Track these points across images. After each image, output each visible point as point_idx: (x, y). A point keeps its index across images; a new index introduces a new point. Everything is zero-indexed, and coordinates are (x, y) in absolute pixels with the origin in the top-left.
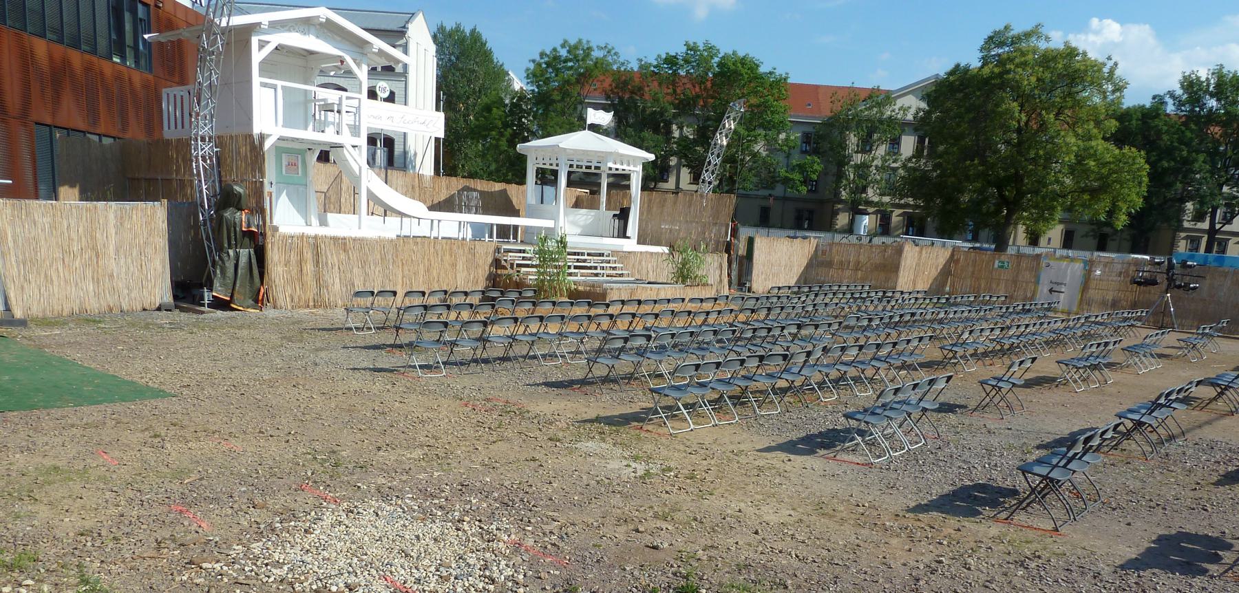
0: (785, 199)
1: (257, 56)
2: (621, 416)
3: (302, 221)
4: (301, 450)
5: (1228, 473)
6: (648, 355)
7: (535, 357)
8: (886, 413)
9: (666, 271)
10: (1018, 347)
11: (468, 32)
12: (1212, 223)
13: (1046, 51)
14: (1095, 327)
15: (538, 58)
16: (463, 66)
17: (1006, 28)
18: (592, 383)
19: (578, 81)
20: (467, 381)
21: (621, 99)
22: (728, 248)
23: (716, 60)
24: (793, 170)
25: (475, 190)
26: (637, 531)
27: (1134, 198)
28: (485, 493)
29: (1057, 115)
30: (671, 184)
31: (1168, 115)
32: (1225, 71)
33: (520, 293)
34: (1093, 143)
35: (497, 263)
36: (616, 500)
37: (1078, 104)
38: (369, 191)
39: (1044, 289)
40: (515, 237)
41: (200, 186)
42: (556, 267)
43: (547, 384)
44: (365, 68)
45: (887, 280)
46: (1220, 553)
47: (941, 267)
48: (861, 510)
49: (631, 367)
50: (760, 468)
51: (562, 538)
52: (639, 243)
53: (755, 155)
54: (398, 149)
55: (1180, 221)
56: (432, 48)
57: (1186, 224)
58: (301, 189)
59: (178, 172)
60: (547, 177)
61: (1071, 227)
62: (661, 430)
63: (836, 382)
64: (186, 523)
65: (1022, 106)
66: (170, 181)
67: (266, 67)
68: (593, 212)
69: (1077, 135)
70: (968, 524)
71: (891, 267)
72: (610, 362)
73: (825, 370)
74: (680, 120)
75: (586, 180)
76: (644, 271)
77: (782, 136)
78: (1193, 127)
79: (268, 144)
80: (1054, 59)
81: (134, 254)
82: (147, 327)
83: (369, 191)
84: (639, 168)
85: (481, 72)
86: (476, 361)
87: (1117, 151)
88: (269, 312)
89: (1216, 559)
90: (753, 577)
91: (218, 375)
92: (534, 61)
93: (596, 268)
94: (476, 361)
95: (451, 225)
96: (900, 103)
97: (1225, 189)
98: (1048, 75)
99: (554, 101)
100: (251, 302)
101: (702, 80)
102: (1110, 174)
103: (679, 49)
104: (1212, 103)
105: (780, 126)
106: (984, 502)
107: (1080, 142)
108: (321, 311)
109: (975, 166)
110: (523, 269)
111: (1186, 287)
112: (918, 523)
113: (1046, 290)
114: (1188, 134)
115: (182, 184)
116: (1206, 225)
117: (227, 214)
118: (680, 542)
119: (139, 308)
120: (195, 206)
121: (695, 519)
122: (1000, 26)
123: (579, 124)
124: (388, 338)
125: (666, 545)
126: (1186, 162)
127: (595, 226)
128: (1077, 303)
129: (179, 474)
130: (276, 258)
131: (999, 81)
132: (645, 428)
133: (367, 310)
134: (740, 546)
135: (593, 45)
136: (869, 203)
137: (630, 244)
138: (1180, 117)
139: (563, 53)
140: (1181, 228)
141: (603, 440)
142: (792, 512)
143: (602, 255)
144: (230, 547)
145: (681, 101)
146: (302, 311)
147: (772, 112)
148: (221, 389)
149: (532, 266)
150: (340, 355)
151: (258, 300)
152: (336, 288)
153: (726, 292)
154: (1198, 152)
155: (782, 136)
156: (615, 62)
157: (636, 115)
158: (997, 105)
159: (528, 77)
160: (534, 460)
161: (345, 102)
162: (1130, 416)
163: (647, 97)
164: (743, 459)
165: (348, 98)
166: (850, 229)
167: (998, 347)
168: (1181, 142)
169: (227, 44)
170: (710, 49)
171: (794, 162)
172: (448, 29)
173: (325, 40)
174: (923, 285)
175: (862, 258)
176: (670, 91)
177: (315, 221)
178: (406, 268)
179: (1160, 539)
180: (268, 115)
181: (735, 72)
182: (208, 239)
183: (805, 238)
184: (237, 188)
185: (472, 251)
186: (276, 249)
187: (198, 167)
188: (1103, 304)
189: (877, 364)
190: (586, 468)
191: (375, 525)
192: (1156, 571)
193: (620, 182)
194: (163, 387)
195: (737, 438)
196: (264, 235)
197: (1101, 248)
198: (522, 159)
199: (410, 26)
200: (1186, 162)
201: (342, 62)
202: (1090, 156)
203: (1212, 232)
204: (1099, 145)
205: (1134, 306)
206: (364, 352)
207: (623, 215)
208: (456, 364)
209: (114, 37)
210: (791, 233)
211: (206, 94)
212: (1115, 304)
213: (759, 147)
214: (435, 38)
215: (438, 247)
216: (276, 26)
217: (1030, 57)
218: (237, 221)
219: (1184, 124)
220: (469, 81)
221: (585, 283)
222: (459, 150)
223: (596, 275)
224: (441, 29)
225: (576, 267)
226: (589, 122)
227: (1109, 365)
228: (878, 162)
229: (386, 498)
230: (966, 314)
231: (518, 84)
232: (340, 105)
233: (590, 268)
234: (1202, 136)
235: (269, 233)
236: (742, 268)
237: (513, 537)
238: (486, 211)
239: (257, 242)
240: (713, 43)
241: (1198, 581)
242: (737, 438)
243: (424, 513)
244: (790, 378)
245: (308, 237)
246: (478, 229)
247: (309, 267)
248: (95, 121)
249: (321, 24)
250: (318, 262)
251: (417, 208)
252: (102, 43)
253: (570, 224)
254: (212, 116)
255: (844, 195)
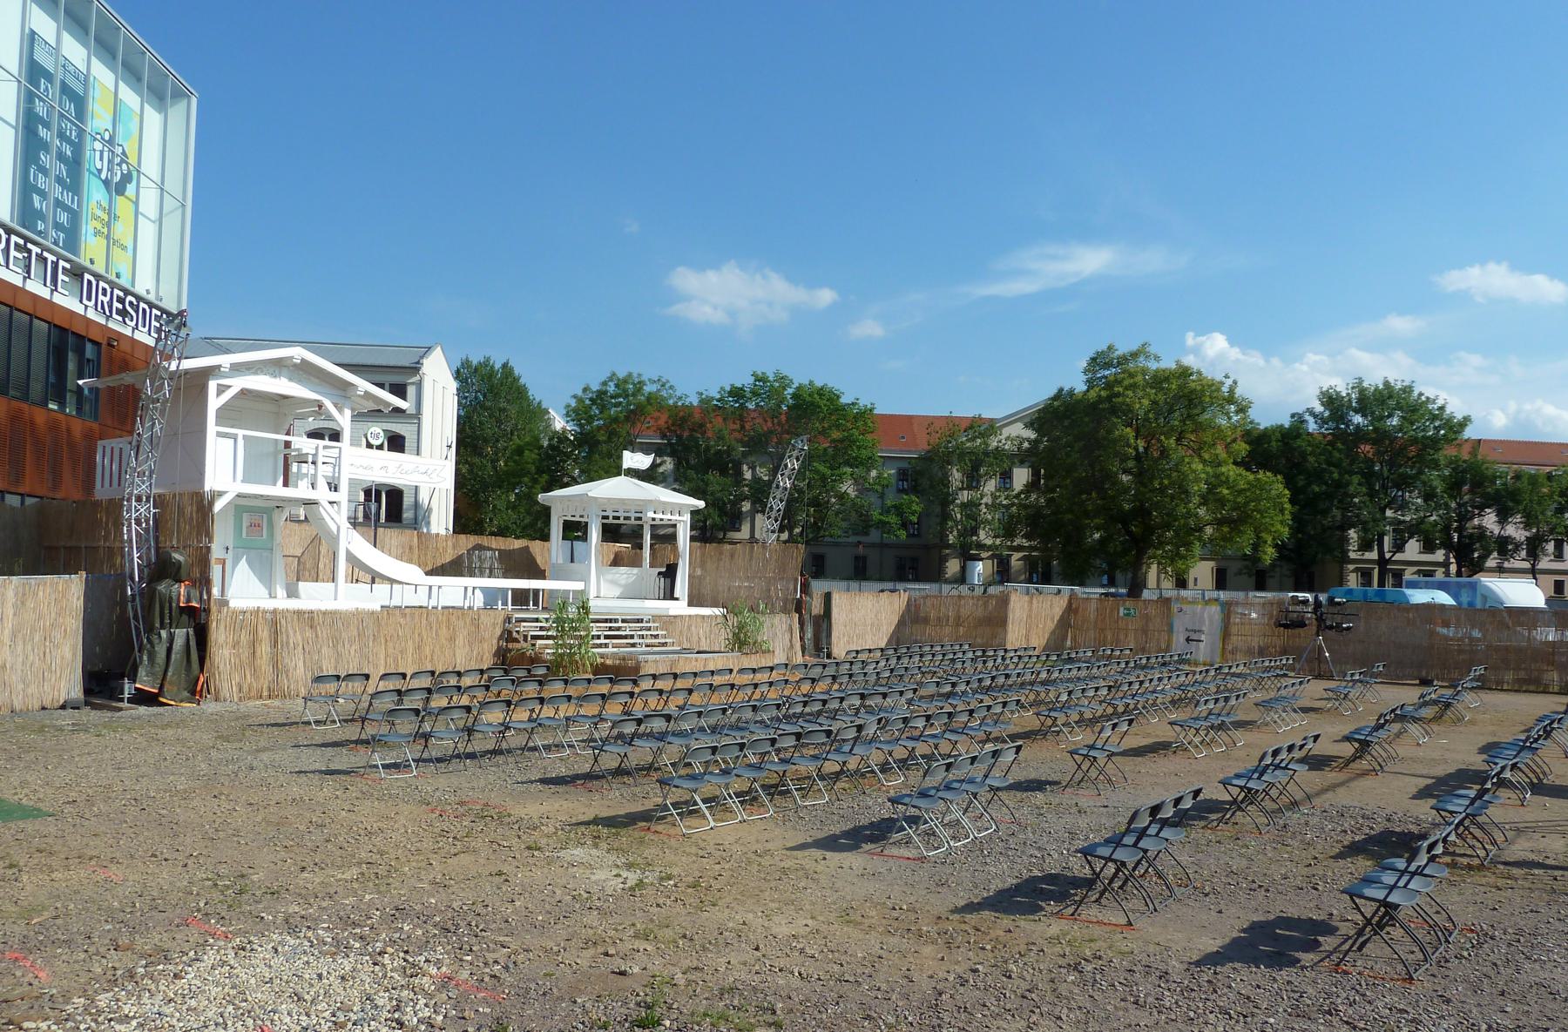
0: (882, 546)
1: (214, 403)
2: (628, 815)
3: (264, 592)
4: (201, 875)
5: (1353, 843)
6: (670, 739)
7: (535, 749)
8: (940, 794)
9: (721, 638)
10: (1136, 708)
11: (498, 366)
12: (1381, 553)
13: (1157, 371)
14: (1231, 682)
15: (580, 393)
16: (490, 402)
17: (1110, 348)
18: (603, 777)
19: (627, 418)
20: (442, 782)
21: (679, 437)
22: (799, 607)
23: (790, 391)
24: (888, 512)
25: (489, 549)
26: (607, 954)
27: (1280, 526)
28: (424, 918)
29: (1178, 440)
30: (744, 533)
31: (1309, 434)
32: (1365, 384)
33: (529, 671)
34: (1224, 469)
35: (508, 636)
36: (592, 918)
37: (1199, 428)
38: (348, 553)
39: (1179, 639)
40: (536, 604)
41: (131, 554)
42: (576, 637)
43: (543, 781)
44: (348, 413)
45: (994, 636)
46: (1320, 939)
47: (1057, 618)
48: (895, 914)
49: (641, 752)
50: (784, 871)
51: (506, 968)
52: (690, 604)
53: (842, 497)
54: (408, 501)
55: (1345, 552)
56: (453, 386)
57: (1352, 555)
58: (265, 554)
59: (106, 538)
60: (575, 530)
61: (1223, 564)
62: (672, 831)
63: (903, 764)
64: (18, 973)
65: (1137, 431)
66: (96, 549)
67: (224, 415)
68: (635, 570)
69: (1204, 462)
70: (1024, 923)
71: (997, 620)
72: (622, 751)
73: (886, 748)
74: (751, 459)
75: (621, 533)
76: (695, 639)
77: (874, 473)
78: (1339, 445)
79: (218, 506)
80: (1167, 379)
81: (37, 639)
82: (41, 730)
83: (348, 553)
84: (687, 517)
85: (513, 410)
86: (458, 756)
87: (1251, 477)
88: (209, 706)
89: (1313, 946)
90: (736, 1002)
91: (118, 788)
92: (575, 397)
93: (632, 637)
94: (458, 756)
95: (454, 591)
96: (1006, 432)
97: (1389, 513)
98: (1161, 398)
99: (598, 442)
100: (186, 694)
101: (775, 413)
102: (1247, 504)
103: (745, 380)
104: (1358, 419)
105: (868, 463)
106: (1048, 896)
107: (1209, 469)
108: (276, 703)
109: (1092, 500)
110: (539, 642)
111: (1338, 628)
112: (963, 926)
113: (1182, 639)
114: (1337, 454)
115: (111, 552)
116: (1374, 555)
117: (161, 587)
118: (656, 966)
119: (37, 706)
120: (123, 578)
121: (684, 936)
122: (1103, 347)
123: (615, 470)
124: (352, 732)
125: (636, 970)
126: (1339, 485)
127: (632, 590)
128: (1219, 651)
129: (28, 913)
130: (221, 639)
131: (1107, 406)
132: (653, 828)
133: (334, 698)
134: (733, 965)
135: (645, 378)
136: (980, 546)
137: (679, 607)
138: (1325, 436)
139: (611, 388)
140: (1346, 560)
141: (596, 846)
142: (810, 922)
143: (641, 621)
144: (67, 1001)
145: (752, 438)
146: (251, 703)
147: (859, 448)
148: (117, 804)
149: (548, 638)
150: (287, 757)
151: (195, 692)
152: (299, 672)
153: (799, 659)
154: (1351, 473)
155: (874, 473)
156: (671, 397)
157: (698, 455)
158: (1109, 432)
159: (567, 415)
160: (500, 874)
161: (321, 452)
162: (1235, 782)
163: (710, 434)
164: (766, 861)
165: (325, 447)
166: (962, 578)
167: (1110, 710)
168: (1330, 464)
169: (176, 391)
170: (783, 381)
171: (889, 503)
172: (475, 363)
173: (299, 382)
174: (1038, 641)
175: (965, 612)
176: (737, 427)
177: (281, 592)
178: (390, 644)
179: (1254, 927)
180: (225, 468)
181: (812, 404)
182: (136, 617)
183: (892, 591)
184: (176, 556)
185: (476, 623)
186: (222, 627)
187: (129, 531)
188: (1250, 652)
189: (953, 737)
190: (564, 881)
191: (270, 963)
192: (1238, 965)
193: (664, 536)
194: (40, 805)
195: (766, 835)
196: (207, 611)
197: (1260, 587)
198: (546, 512)
199: (425, 361)
200: (1339, 485)
201: (320, 407)
202: (1222, 483)
203: (1382, 562)
204: (1230, 470)
205: (1284, 652)
206: (319, 751)
207: (670, 573)
208: (430, 760)
209: (52, 379)
210: (890, 585)
211: (145, 447)
212: (1262, 652)
213: (848, 487)
214: (458, 375)
215: (432, 618)
216: (238, 369)
217: (1139, 378)
218: (174, 595)
219: (1330, 443)
220: (499, 421)
221: (614, 655)
222: (486, 502)
223: (633, 645)
224: (466, 364)
225: (607, 637)
226: (625, 466)
227: (1239, 725)
228: (987, 500)
229: (293, 930)
230: (1075, 672)
231: (559, 423)
232: (315, 455)
233: (625, 637)
234: (1354, 458)
235: (214, 608)
236: (819, 630)
237: (444, 969)
238: (508, 573)
239: (198, 622)
240: (785, 372)
241: (1284, 974)
242: (766, 835)
243: (337, 946)
244: (840, 758)
245: (265, 612)
246: (491, 596)
247: (264, 649)
248: (18, 478)
249: (295, 365)
250: (276, 642)
251: (411, 572)
252: (37, 388)
253: (604, 588)
254: (151, 472)
255: (951, 539)
